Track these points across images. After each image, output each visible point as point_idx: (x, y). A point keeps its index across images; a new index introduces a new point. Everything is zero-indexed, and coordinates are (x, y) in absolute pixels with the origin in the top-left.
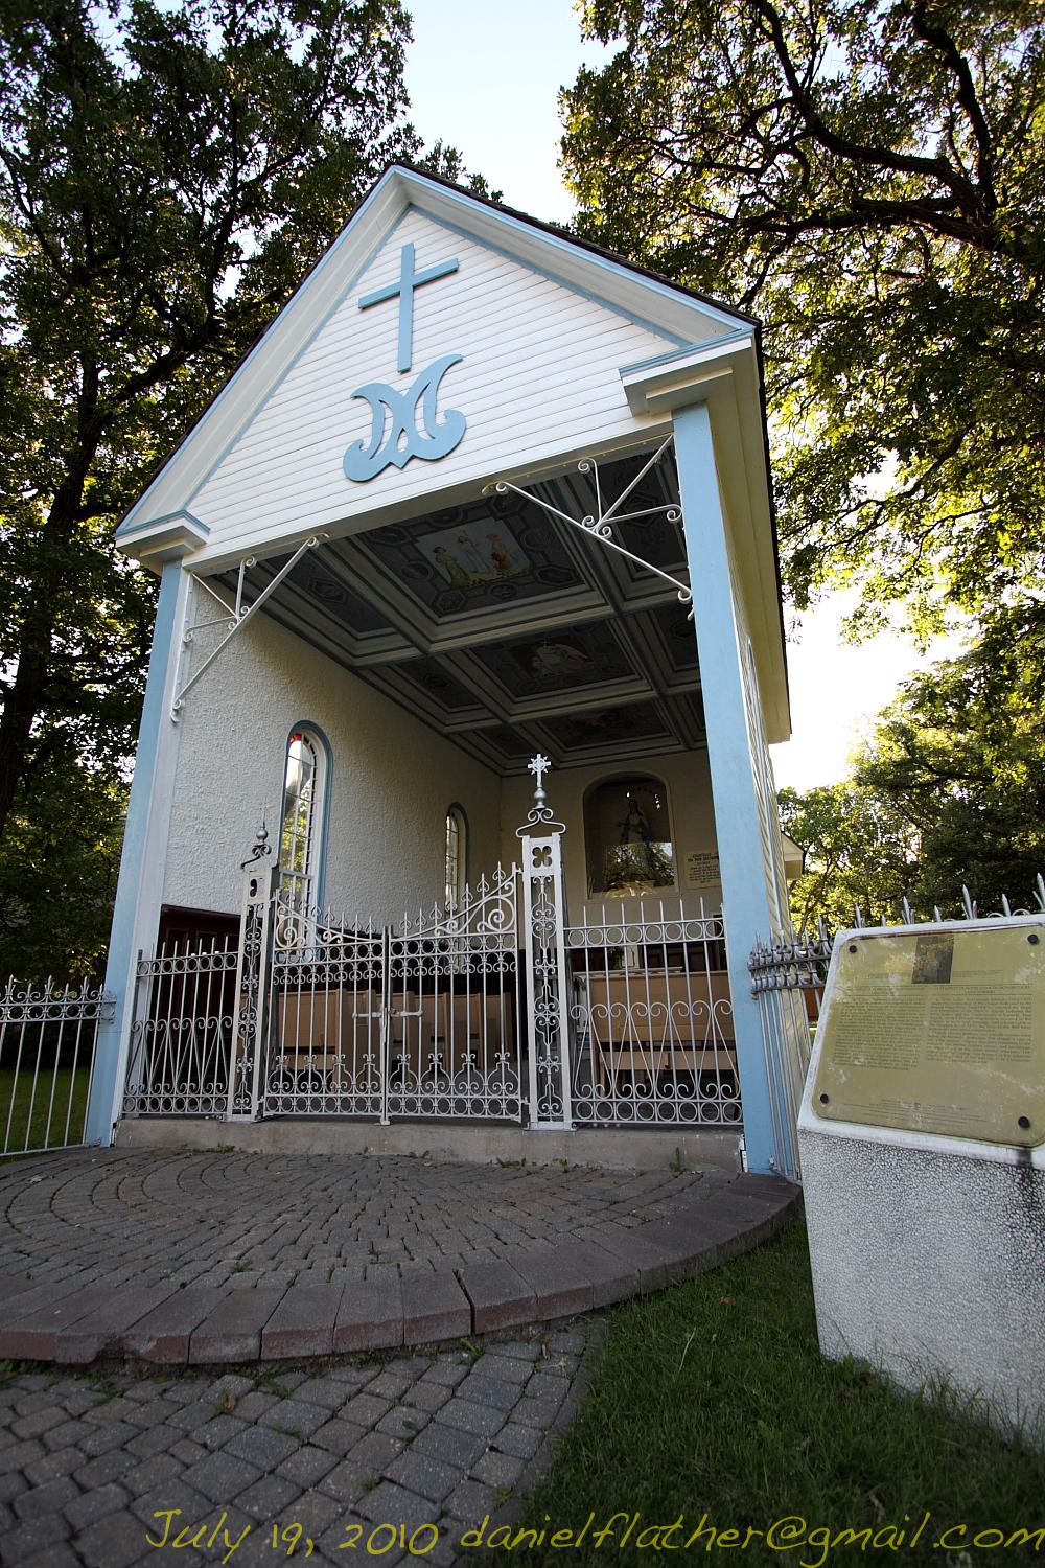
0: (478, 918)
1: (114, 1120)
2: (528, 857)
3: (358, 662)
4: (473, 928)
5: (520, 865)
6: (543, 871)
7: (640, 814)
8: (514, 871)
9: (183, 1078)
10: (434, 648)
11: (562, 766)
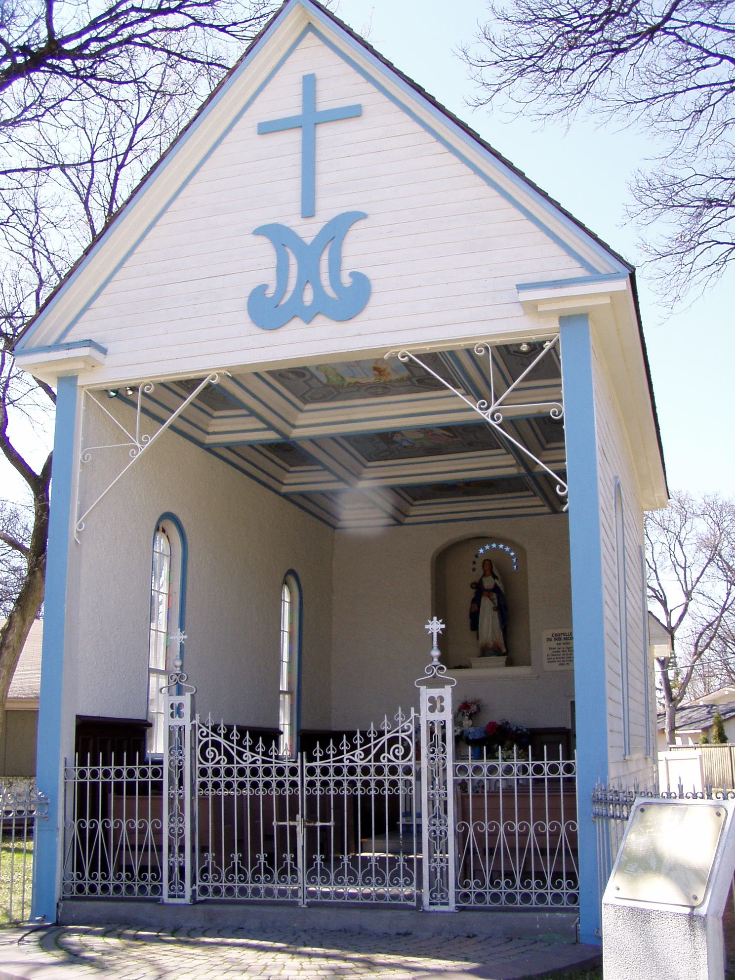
0: (381, 751)
1: (57, 901)
2: (425, 705)
3: (209, 440)
4: (377, 758)
5: (418, 711)
6: (437, 716)
7: (495, 577)
8: (413, 714)
9: (94, 868)
10: (295, 433)
11: (408, 520)
